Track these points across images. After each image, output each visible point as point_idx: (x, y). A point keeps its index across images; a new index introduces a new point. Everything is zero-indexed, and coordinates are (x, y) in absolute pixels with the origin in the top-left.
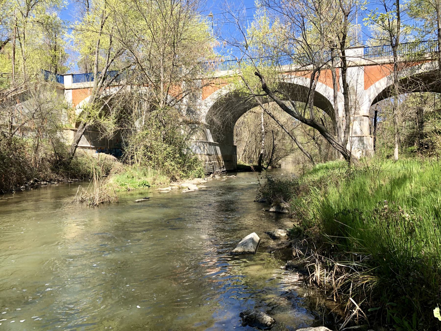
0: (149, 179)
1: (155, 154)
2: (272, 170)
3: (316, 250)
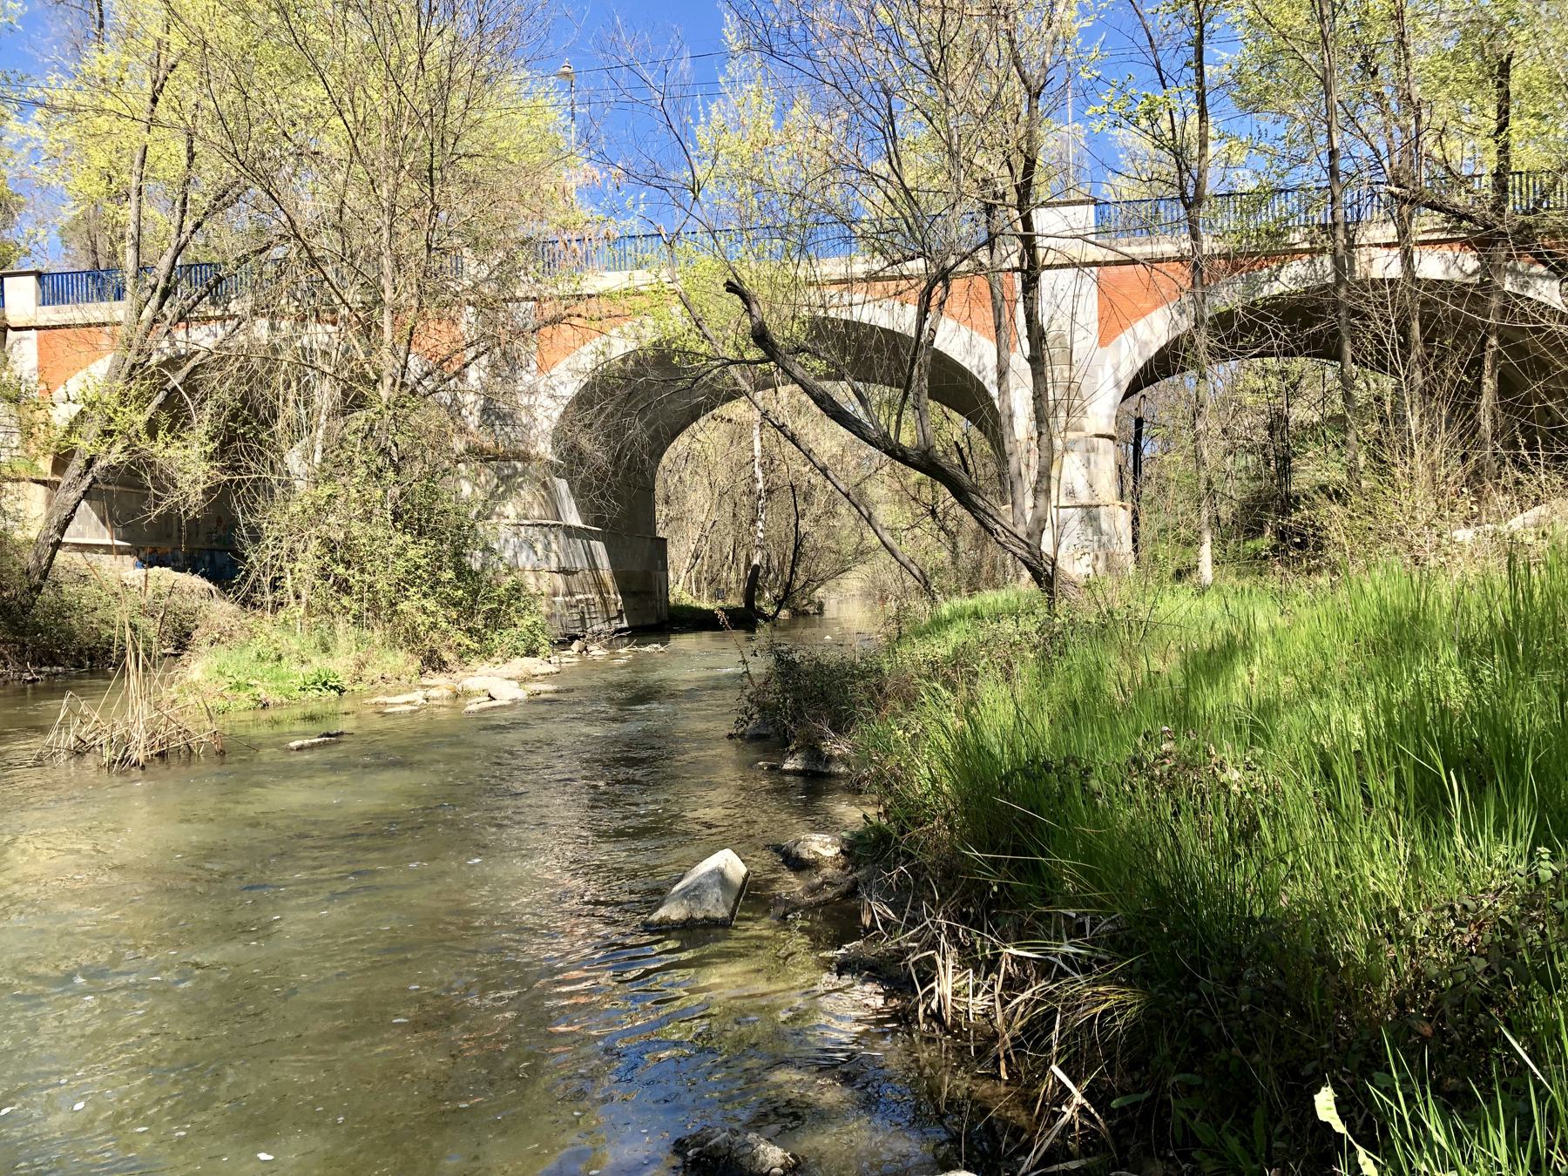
0: (340, 665)
1: (362, 571)
2: (791, 624)
3: (941, 902)
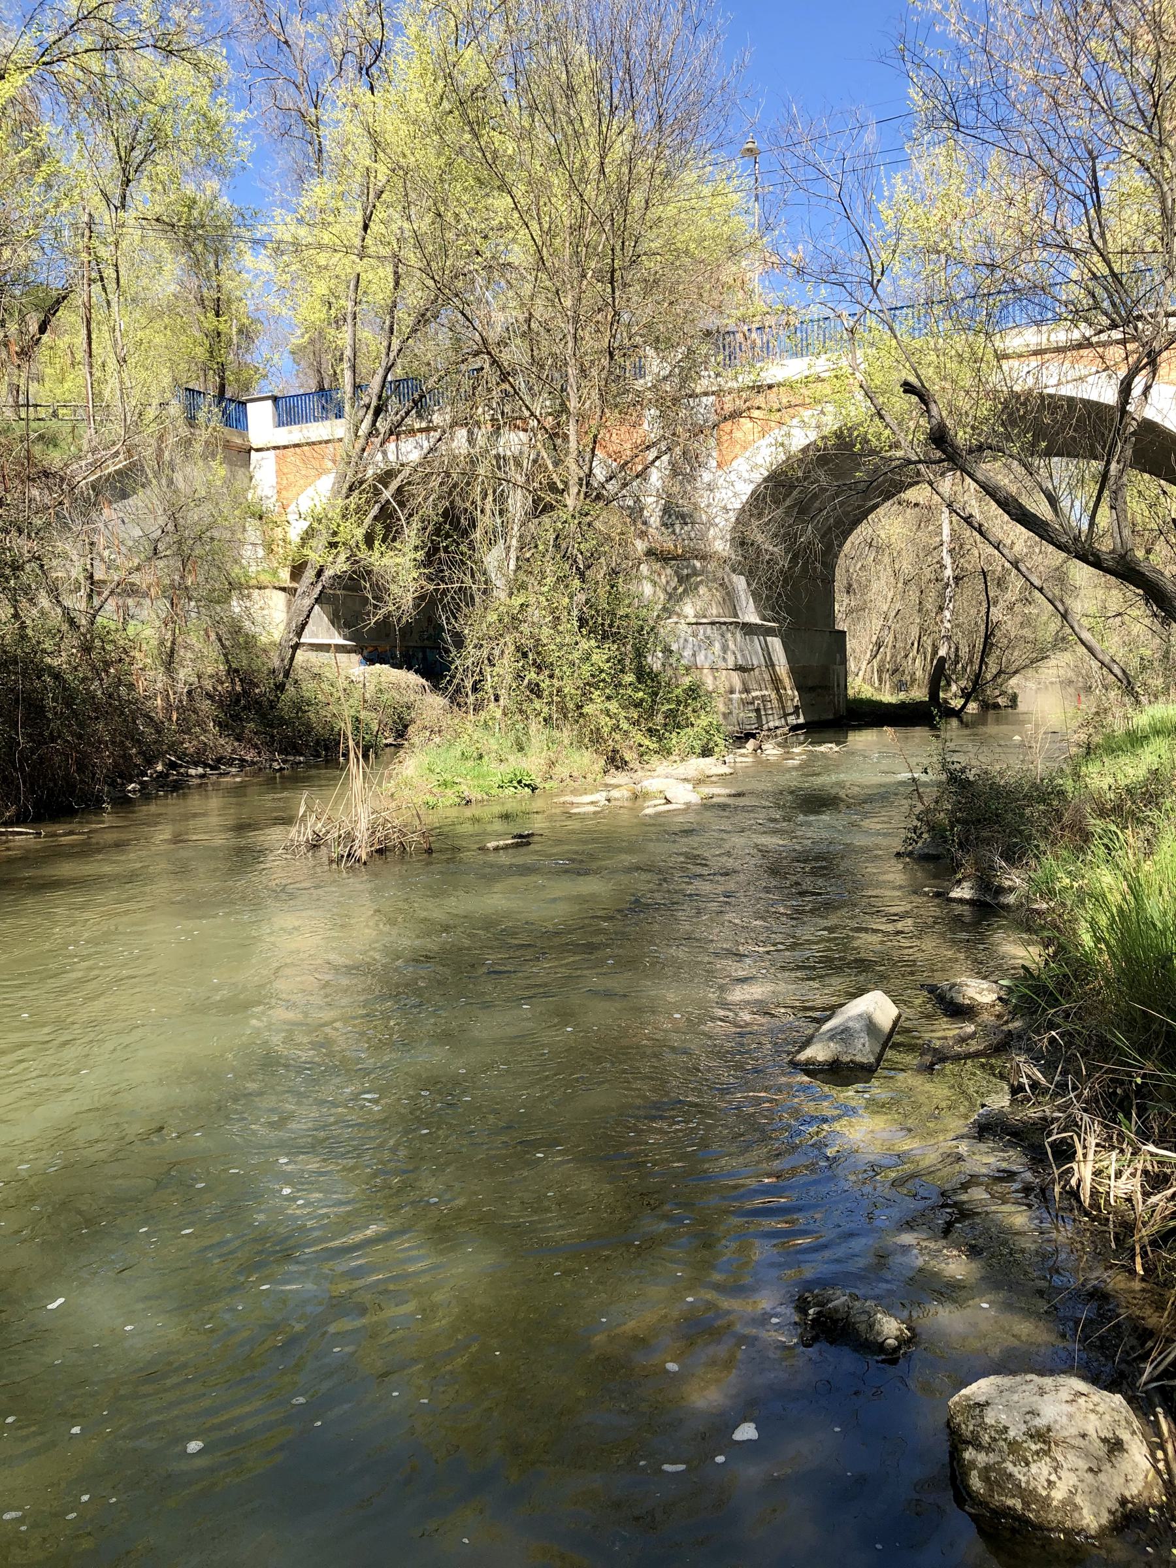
0: (532, 764)
2: (980, 720)
3: (1089, 1076)
